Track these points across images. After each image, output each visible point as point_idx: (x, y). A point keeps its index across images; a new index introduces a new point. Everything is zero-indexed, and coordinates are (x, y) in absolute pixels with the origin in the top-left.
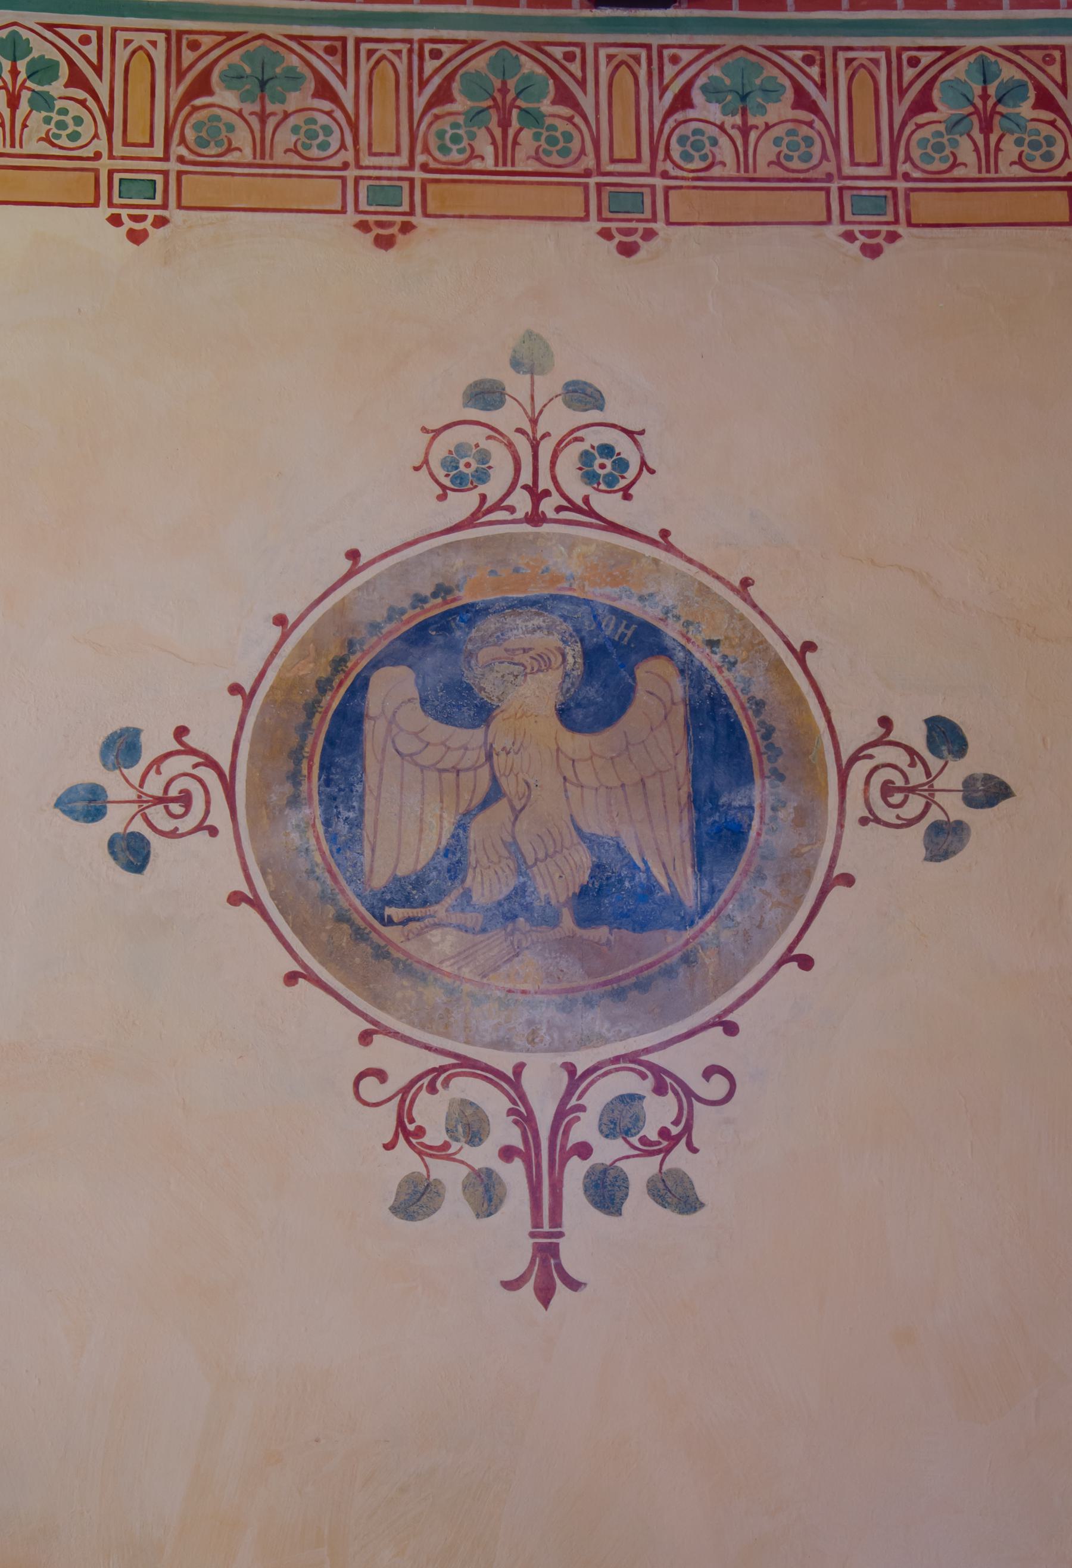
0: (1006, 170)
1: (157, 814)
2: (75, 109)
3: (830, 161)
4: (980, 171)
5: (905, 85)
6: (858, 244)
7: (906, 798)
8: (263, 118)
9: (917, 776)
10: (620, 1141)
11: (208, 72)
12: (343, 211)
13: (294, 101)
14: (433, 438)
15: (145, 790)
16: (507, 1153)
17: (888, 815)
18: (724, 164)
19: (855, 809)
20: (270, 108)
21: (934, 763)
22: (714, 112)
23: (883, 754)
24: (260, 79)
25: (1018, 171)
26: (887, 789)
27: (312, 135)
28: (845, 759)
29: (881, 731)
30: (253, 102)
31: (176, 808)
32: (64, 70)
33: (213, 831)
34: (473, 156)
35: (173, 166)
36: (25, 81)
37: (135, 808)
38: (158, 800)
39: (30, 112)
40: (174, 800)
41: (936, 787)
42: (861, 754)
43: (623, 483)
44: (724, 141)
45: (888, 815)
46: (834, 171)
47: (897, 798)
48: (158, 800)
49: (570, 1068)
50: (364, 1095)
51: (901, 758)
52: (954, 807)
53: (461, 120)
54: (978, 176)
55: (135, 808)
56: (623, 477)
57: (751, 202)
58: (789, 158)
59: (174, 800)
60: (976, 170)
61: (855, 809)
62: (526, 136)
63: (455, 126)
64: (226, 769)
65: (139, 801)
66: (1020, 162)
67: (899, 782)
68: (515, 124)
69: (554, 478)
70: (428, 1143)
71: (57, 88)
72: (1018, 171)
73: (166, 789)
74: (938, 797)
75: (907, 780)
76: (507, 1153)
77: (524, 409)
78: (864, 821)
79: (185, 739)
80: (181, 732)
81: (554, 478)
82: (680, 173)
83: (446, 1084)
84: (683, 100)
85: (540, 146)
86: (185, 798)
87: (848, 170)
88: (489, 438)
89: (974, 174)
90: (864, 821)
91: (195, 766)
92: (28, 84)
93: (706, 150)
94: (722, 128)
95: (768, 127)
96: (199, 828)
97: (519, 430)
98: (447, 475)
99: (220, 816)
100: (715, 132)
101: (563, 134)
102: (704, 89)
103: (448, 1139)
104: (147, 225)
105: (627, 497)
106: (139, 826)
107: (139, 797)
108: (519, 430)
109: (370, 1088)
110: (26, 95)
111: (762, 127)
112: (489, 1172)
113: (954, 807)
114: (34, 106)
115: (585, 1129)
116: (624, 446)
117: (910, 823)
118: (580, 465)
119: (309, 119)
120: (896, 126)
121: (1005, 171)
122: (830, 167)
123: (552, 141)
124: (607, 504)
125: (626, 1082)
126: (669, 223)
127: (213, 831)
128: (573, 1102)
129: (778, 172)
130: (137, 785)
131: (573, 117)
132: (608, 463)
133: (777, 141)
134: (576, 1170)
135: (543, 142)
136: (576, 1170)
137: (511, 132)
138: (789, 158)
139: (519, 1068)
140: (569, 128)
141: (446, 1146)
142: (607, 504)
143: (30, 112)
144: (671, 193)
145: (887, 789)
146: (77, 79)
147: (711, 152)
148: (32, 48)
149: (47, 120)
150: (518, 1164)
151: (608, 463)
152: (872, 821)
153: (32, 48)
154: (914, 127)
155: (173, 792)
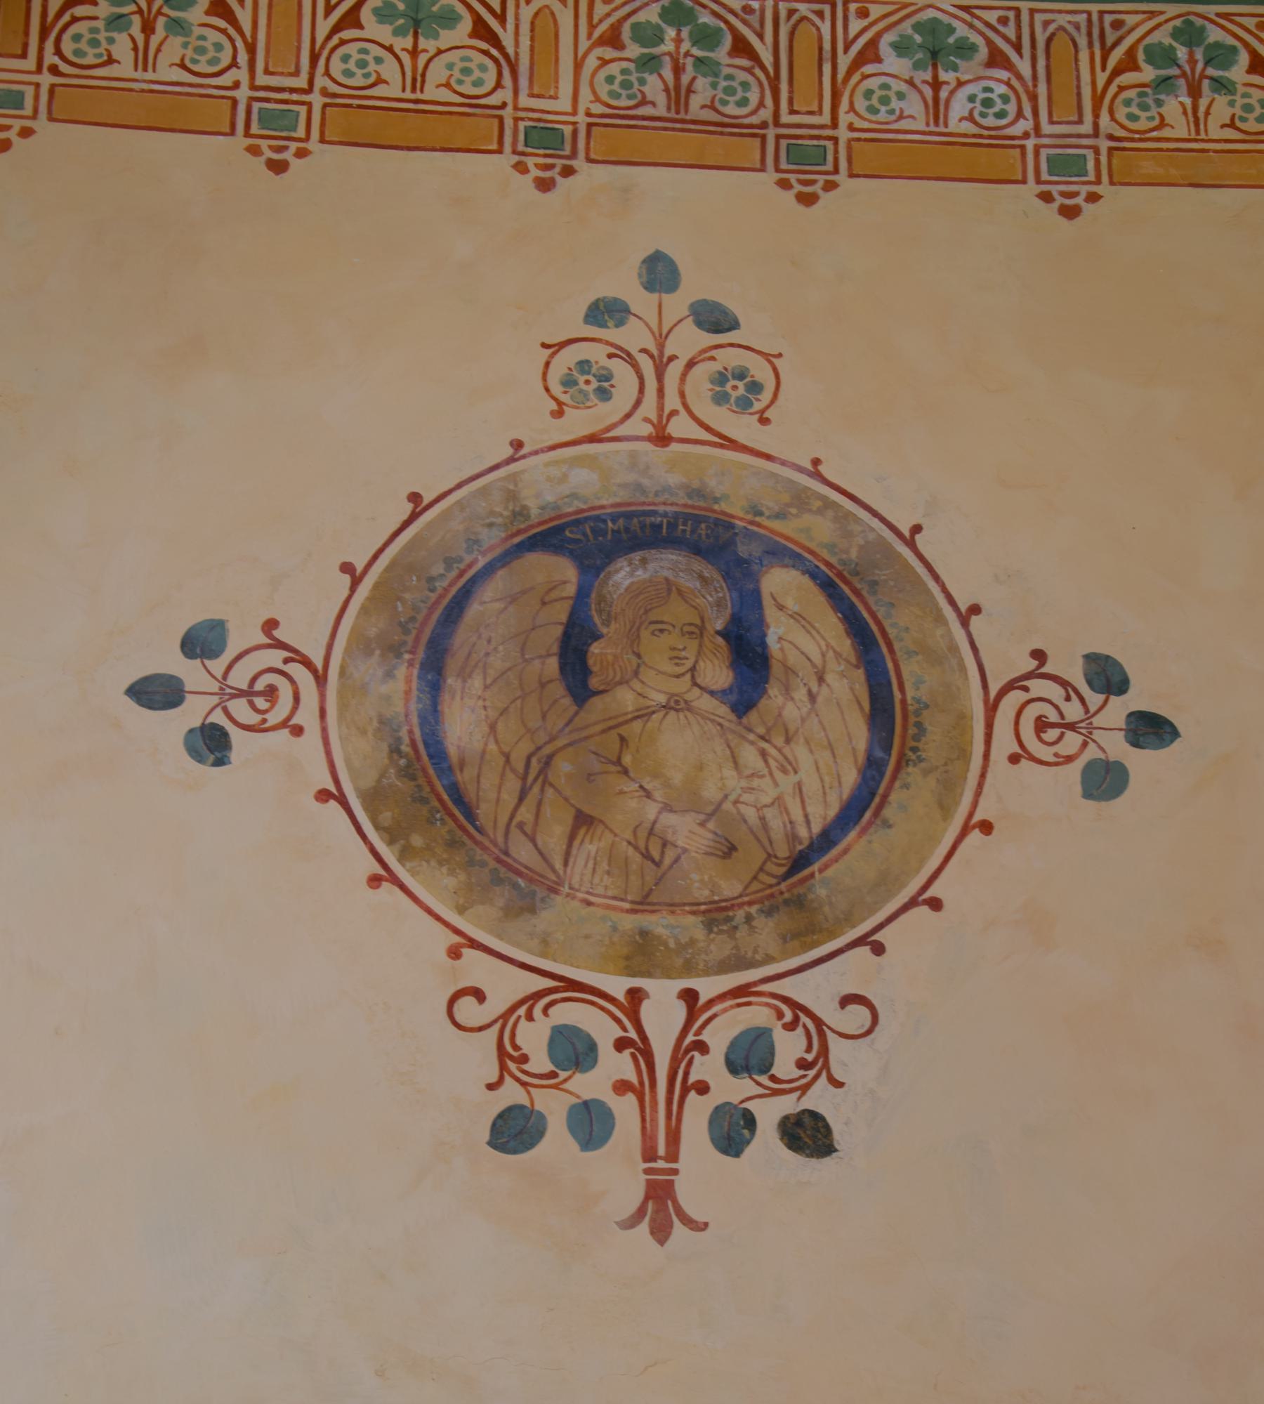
0: (954, 125)
1: (240, 709)
2: (215, 36)
3: (1027, 120)
4: (928, 124)
5: (498, 10)
6: (1056, 205)
7: (1062, 735)
8: (414, 53)
9: (1073, 711)
10: (748, 1081)
11: (873, 43)
12: (232, 132)
13: (448, 38)
14: (554, 353)
15: (230, 682)
16: (622, 1087)
17: (1045, 753)
18: (653, 104)
19: (1004, 743)
20: (943, 76)
21: (1094, 699)
22: (384, 33)
23: (1039, 687)
24: (931, 49)
25: (967, 127)
26: (1041, 725)
27: (987, 103)
28: (993, 693)
29: (1034, 664)
30: (925, 71)
31: (261, 703)
32: (728, 41)
33: (298, 731)
34: (644, 102)
35: (1104, 145)
36: (161, 7)
37: (216, 700)
38: (241, 693)
39: (167, 37)
40: (259, 694)
41: (1095, 724)
42: (1016, 685)
43: (757, 406)
44: (914, 97)
45: (1045, 753)
46: (510, 101)
47: (1052, 734)
48: (241, 693)
49: (689, 996)
50: (458, 1018)
51: (1054, 691)
52: (1116, 746)
53: (100, 24)
54: (927, 129)
55: (215, 700)
56: (758, 400)
57: (718, 146)
58: (725, 103)
59: (259, 694)
60: (924, 123)
61: (1004, 743)
62: (701, 83)
63: (94, 30)
64: (319, 664)
65: (221, 692)
66: (970, 118)
67: (1053, 717)
68: (690, 71)
69: (682, 395)
70: (530, 1070)
71: (721, 54)
72: (967, 127)
73: (254, 680)
74: (1097, 735)
75: (1062, 715)
76: (622, 1087)
77: (650, 329)
78: (1014, 759)
79: (276, 633)
80: (270, 625)
81: (682, 395)
82: (866, 125)
83: (545, 1011)
84: (870, 54)
85: (975, 107)
86: (271, 693)
87: (786, 118)
88: (610, 356)
89: (922, 127)
90: (1014, 759)
91: (286, 661)
92: (166, 10)
93: (635, 90)
94: (910, 82)
95: (960, 84)
96: (284, 724)
97: (644, 351)
98: (565, 392)
99: (307, 716)
100: (904, 87)
101: (1001, 96)
102: (376, 11)
103: (554, 1068)
104: (817, 188)
105: (764, 421)
106: (218, 718)
107: (221, 689)
108: (644, 351)
109: (468, 1010)
110: (161, 21)
111: (954, 84)
112: (600, 1104)
113: (1116, 746)
114: (168, 28)
115: (709, 1067)
116: (760, 371)
117: (1069, 759)
118: (612, 390)
119: (363, 49)
120: (840, 77)
121: (1215, 133)
122: (766, 114)
123: (201, 50)
124: (741, 428)
125: (757, 1015)
126: (590, 160)
127: (298, 731)
128: (690, 1038)
129: (971, 128)
130: (219, 676)
131: (753, 67)
132: (728, 387)
133: (450, 66)
134: (697, 1112)
135: (978, 104)
136: (697, 1112)
137: (155, 40)
138: (725, 103)
139: (636, 996)
140: (750, 78)
141: (553, 1075)
142: (741, 428)
143: (167, 37)
144: (594, 129)
145: (1041, 725)
146: (741, 47)
147: (640, 90)
148: (646, 20)
149: (185, 45)
150: (631, 1098)
151: (741, 384)
152: (387, 880)
153: (646, 20)
154: (597, 63)
155: (260, 686)
